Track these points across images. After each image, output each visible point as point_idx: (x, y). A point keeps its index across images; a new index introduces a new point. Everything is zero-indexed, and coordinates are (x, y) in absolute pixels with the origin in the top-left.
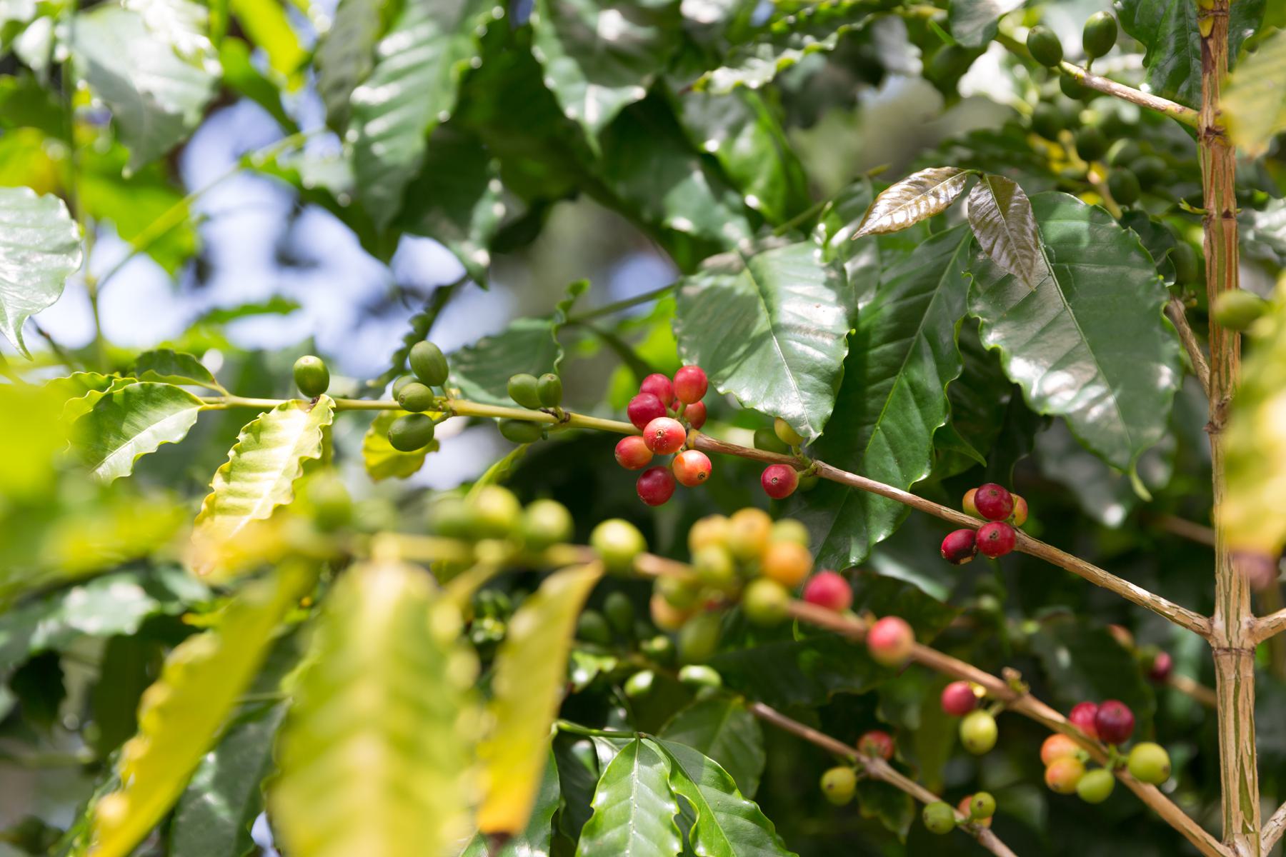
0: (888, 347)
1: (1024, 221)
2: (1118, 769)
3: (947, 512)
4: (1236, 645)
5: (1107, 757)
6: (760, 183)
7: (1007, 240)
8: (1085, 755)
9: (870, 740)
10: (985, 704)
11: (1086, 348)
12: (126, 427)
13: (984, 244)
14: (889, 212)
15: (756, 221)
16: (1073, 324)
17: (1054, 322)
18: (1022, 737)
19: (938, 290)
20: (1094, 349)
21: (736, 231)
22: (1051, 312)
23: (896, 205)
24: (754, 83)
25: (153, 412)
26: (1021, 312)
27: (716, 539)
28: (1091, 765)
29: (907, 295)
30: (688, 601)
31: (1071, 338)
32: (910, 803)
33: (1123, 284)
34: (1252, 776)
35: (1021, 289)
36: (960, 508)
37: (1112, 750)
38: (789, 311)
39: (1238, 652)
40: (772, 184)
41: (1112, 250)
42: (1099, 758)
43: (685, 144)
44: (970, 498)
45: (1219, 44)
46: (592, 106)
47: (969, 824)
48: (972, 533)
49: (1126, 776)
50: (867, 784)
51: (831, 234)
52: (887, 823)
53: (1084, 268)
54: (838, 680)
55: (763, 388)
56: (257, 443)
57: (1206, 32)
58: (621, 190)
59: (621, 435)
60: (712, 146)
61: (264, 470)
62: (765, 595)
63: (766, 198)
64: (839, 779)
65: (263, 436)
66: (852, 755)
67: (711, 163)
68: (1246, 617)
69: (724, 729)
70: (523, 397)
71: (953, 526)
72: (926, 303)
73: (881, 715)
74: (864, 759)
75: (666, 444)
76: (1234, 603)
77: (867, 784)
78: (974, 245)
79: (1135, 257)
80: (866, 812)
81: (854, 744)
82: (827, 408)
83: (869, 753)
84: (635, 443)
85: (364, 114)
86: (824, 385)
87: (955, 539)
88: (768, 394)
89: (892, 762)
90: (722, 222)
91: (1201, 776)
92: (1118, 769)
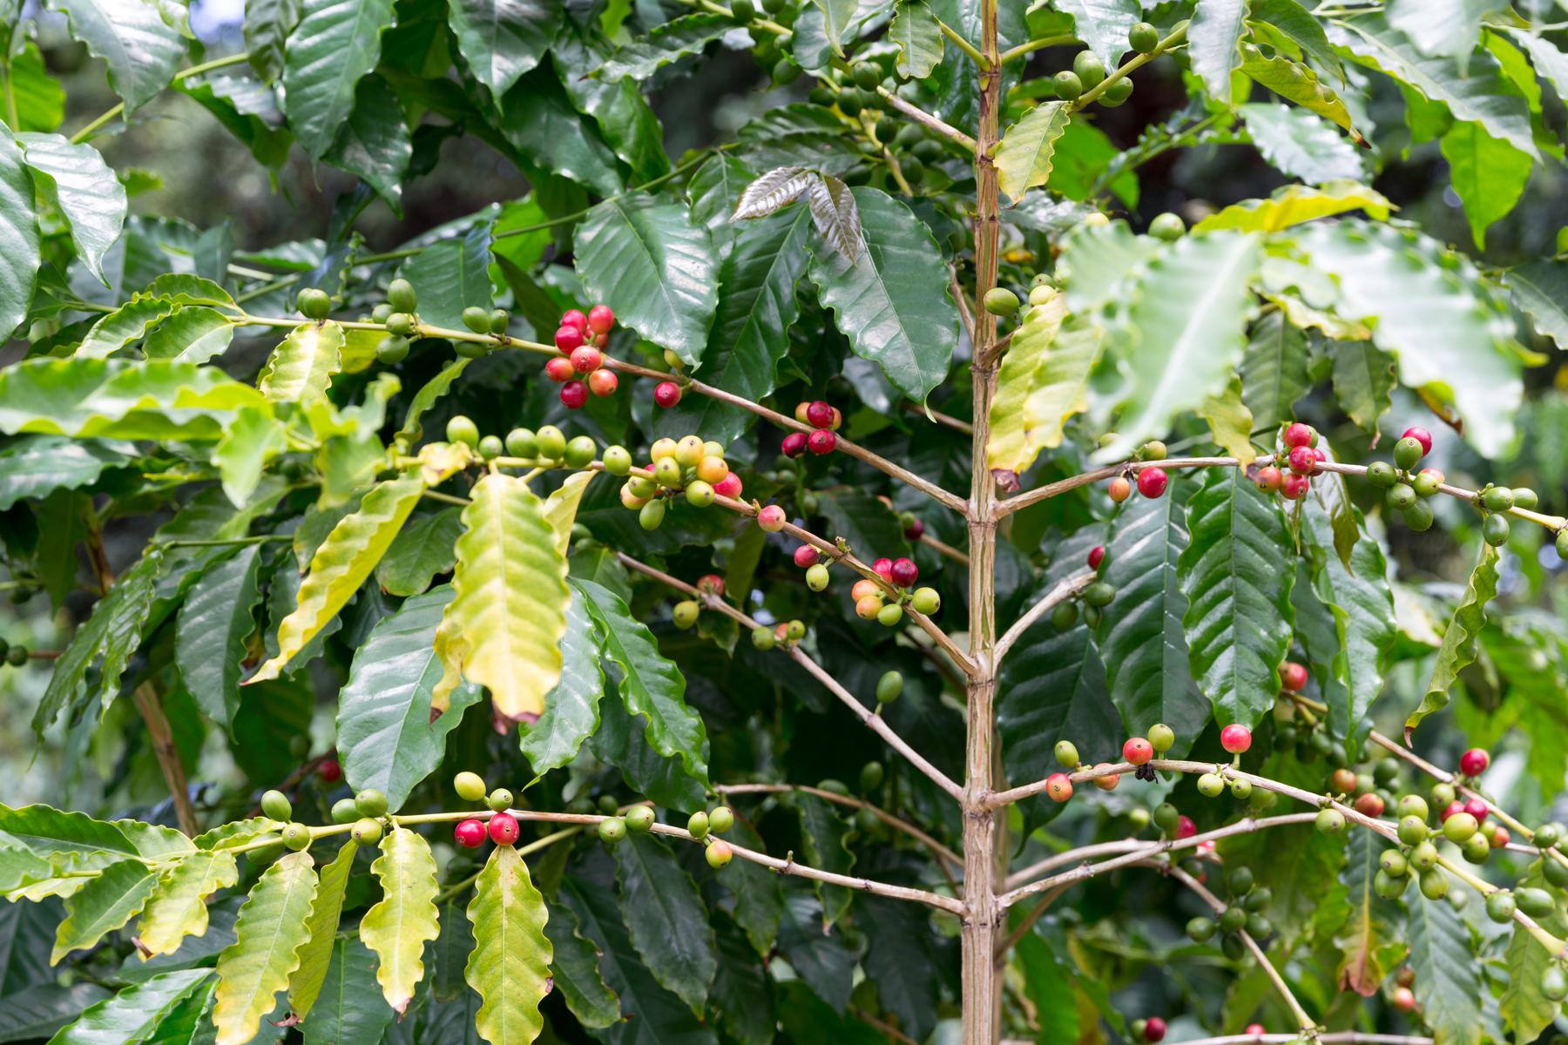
0: (743, 293)
1: (849, 213)
2: (905, 604)
3: (786, 419)
4: (984, 520)
5: (898, 596)
6: (630, 141)
7: (838, 228)
8: (883, 594)
9: (707, 581)
10: (821, 559)
11: (891, 311)
12: (180, 341)
13: (822, 228)
14: (754, 202)
15: (623, 170)
16: (883, 291)
17: (869, 289)
18: (845, 578)
19: (781, 253)
20: (898, 311)
21: (609, 180)
22: (867, 282)
23: (757, 198)
24: (639, 76)
25: (197, 329)
26: (845, 279)
27: (667, 453)
28: (887, 601)
29: (756, 255)
30: (652, 491)
31: (881, 301)
32: (736, 628)
33: (918, 264)
34: (990, 610)
35: (845, 261)
36: (793, 416)
37: (902, 591)
38: (672, 263)
39: (986, 526)
40: (638, 144)
41: (911, 236)
42: (892, 597)
43: (568, 104)
44: (803, 409)
45: (992, 97)
46: (499, 70)
47: (785, 644)
48: (805, 437)
49: (911, 608)
50: (707, 613)
51: (697, 198)
52: (719, 643)
53: (892, 249)
54: (686, 536)
55: (656, 324)
56: (286, 359)
57: (984, 87)
58: (515, 140)
59: (553, 356)
60: (590, 108)
61: (293, 379)
62: (699, 490)
63: (634, 156)
64: (687, 610)
65: (291, 352)
66: (696, 592)
67: (589, 122)
68: (992, 501)
69: (598, 570)
70: (475, 325)
71: (793, 430)
72: (771, 261)
73: (714, 563)
74: (704, 595)
75: (587, 367)
76: (984, 490)
77: (707, 613)
78: (812, 226)
79: (927, 244)
80: (703, 635)
81: (694, 584)
82: (703, 344)
83: (707, 590)
84: (561, 363)
85: (293, 60)
86: (701, 325)
87: (793, 440)
88: (660, 330)
89: (723, 597)
90: (599, 174)
91: (953, 615)
92: (905, 604)
